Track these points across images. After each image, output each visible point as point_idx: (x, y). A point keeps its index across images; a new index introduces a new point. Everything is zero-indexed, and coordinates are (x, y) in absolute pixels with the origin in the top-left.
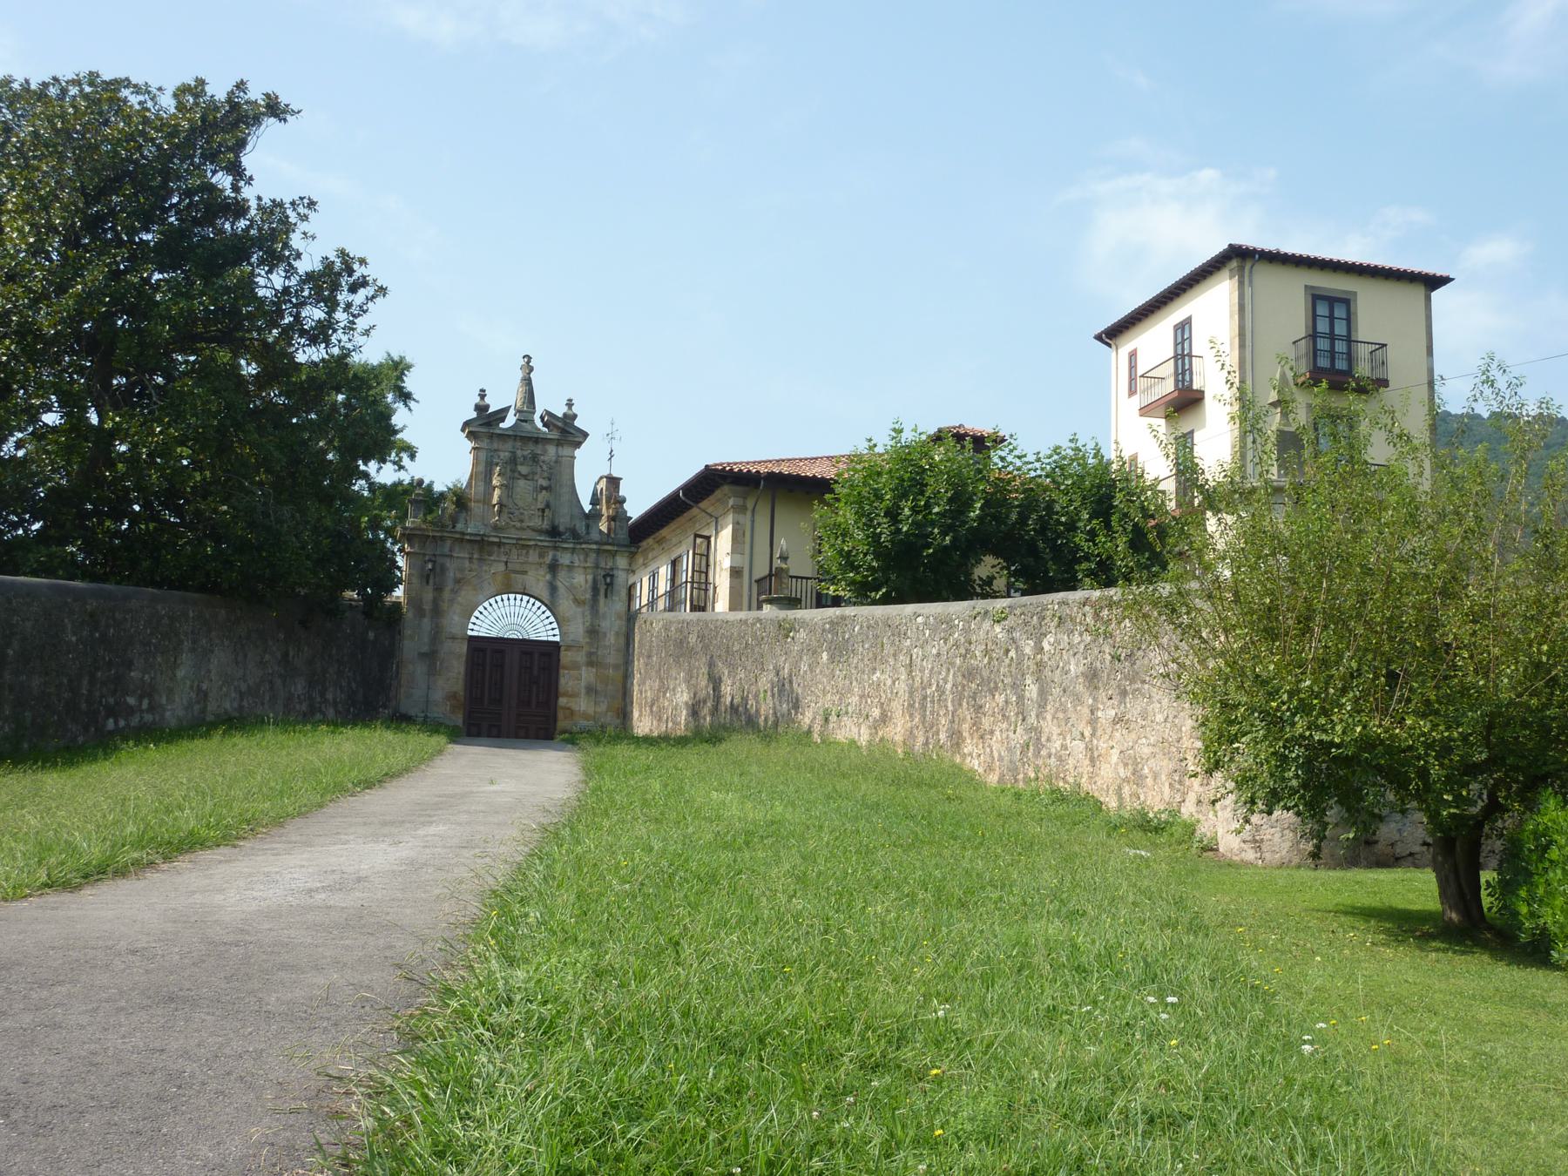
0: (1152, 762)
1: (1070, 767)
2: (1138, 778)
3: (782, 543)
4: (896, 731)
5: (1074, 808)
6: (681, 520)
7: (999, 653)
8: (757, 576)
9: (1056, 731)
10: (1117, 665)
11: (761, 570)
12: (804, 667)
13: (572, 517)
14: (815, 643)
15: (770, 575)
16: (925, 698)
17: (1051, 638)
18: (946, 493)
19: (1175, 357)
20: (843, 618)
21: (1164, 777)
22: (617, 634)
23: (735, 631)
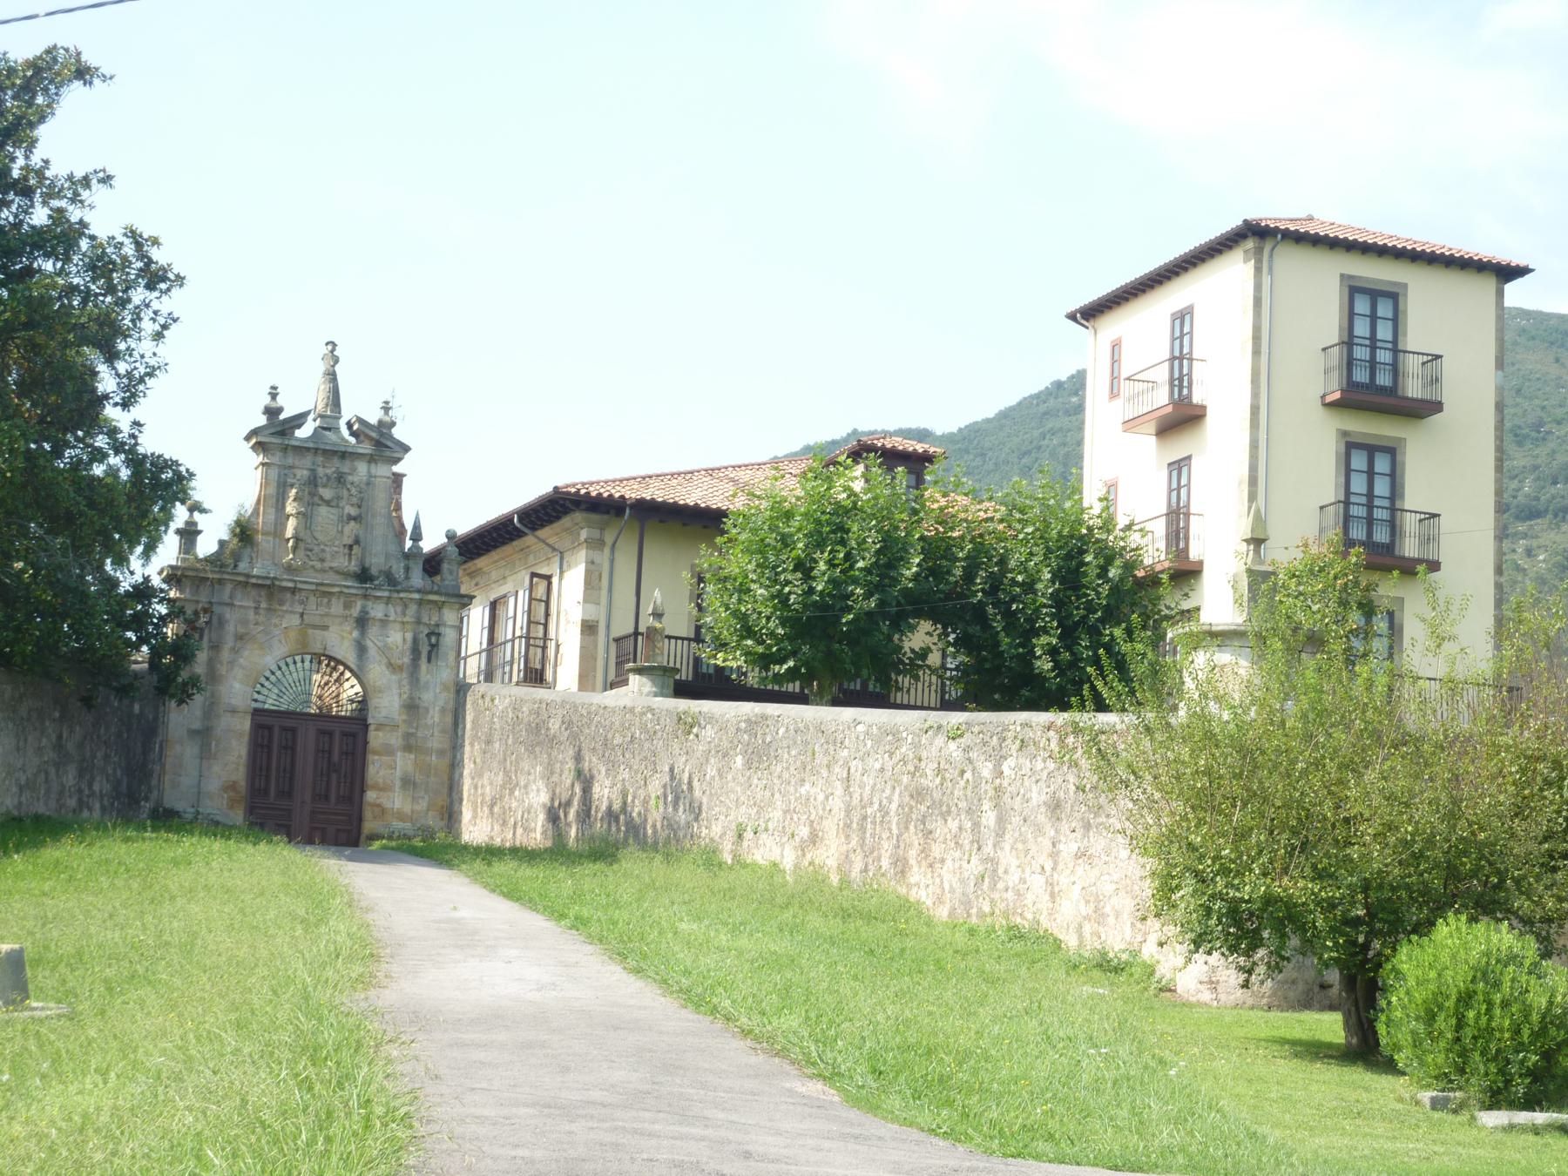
0: (1114, 900)
1: (1028, 902)
2: (1099, 916)
3: (655, 596)
4: (829, 855)
5: (1030, 946)
6: (507, 550)
7: (952, 773)
8: (616, 633)
9: (1014, 862)
10: (1081, 796)
11: (623, 626)
12: (711, 771)
13: (387, 556)
14: (725, 744)
15: (636, 633)
16: (865, 818)
17: (1011, 762)
18: (873, 541)
19: (1173, 359)
20: (764, 717)
21: (1125, 916)
22: (443, 711)
23: (617, 720)
